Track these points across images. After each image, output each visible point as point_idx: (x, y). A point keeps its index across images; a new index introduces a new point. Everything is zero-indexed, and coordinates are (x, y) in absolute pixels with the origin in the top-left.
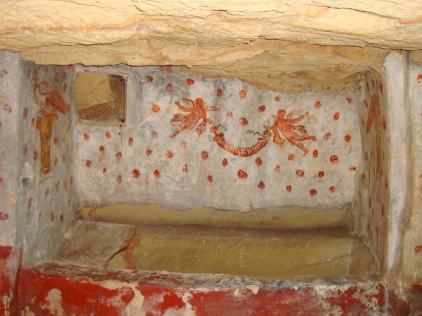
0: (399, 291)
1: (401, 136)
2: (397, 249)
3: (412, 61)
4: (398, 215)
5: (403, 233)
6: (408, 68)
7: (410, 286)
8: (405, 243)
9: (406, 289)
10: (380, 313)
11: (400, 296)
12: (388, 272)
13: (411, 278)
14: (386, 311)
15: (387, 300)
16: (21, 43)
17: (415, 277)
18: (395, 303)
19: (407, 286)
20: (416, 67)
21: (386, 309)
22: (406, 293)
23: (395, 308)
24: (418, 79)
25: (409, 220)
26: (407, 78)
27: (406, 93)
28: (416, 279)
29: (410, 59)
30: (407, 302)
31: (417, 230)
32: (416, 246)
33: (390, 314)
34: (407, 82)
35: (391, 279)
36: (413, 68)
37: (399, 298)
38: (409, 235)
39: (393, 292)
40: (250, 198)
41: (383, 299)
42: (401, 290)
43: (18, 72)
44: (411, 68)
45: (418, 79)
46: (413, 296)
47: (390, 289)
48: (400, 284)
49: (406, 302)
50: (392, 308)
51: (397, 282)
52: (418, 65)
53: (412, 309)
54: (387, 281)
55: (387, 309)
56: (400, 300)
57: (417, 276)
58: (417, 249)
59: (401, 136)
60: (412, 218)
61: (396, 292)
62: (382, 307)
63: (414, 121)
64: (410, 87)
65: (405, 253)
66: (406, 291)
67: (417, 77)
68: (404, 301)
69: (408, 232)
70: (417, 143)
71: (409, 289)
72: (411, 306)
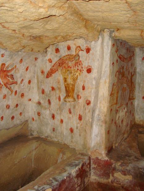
23: (99, 166)
30: (109, 160)
49: (108, 160)
50: (96, 167)
55: (92, 168)
61: (100, 158)
68: (106, 160)
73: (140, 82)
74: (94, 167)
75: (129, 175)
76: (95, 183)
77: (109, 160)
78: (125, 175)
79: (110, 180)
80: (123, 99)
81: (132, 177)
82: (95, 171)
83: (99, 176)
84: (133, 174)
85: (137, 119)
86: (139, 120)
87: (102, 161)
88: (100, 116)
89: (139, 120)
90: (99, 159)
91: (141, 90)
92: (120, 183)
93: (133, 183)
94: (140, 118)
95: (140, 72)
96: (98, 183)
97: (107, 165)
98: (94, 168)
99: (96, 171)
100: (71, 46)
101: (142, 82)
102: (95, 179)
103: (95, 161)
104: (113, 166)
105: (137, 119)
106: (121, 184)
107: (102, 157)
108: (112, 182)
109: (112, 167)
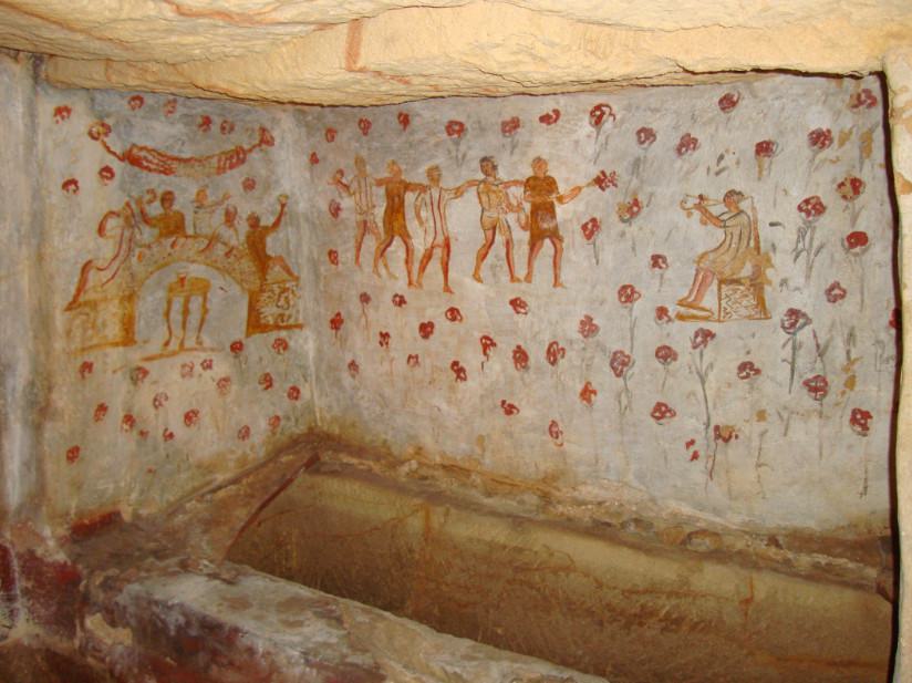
0: (47, 545)
1: (19, 231)
2: (26, 465)
3: (47, 79)
4: (18, 395)
5: (37, 428)
6: (36, 93)
7: (68, 529)
8: (46, 448)
9: (61, 539)
10: (8, 604)
11: (50, 555)
12: (10, 515)
13: (67, 514)
14: (19, 598)
15: (17, 575)
16: (451, 82)
17: (73, 512)
18: (40, 574)
19: (63, 531)
20: (51, 91)
21: (18, 592)
22: (62, 546)
23: (40, 584)
24: (55, 115)
25: (48, 403)
26: (32, 114)
27: (31, 145)
28: (76, 514)
29: (43, 76)
30: (69, 563)
31: (66, 417)
32: (68, 449)
33: (29, 600)
34: (33, 122)
35: (20, 529)
36: (47, 93)
37: (49, 560)
38: (51, 431)
39: (31, 553)
40: (755, 97)
41: (9, 574)
42: (51, 543)
43: (265, 83)
44: (42, 93)
45: (55, 115)
46: (77, 549)
47: (21, 549)
48: (47, 532)
49: (65, 563)
50: (33, 587)
51: (38, 531)
52: (56, 87)
53: (85, 572)
54: (12, 535)
55: (22, 591)
56: (53, 563)
57: (77, 507)
58: (71, 455)
59: (19, 231)
60: (54, 396)
61: (39, 552)
62: (11, 590)
63: (48, 201)
64: (40, 132)
65: (49, 467)
66: (62, 542)
67: (53, 112)
68: (62, 562)
69: (48, 425)
70: (56, 244)
71: (65, 537)
72: (80, 567)
73: (316, 256)
74: (26, 588)
75: (124, 627)
76: (39, 650)
77: (69, 563)
78: (113, 624)
79: (77, 643)
80: (194, 319)
81: (131, 635)
82: (31, 602)
83: (47, 623)
84: (133, 622)
85: (321, 409)
86: (328, 417)
87: (48, 565)
88: (35, 390)
89: (328, 417)
90: (37, 559)
91: (322, 288)
92: (102, 655)
93: (137, 660)
94: (330, 407)
95: (312, 213)
96: (48, 650)
97: (66, 580)
98: (26, 592)
99: (33, 605)
100: (521, 118)
101: (322, 259)
102: (37, 636)
103: (28, 564)
104: (81, 587)
105: (321, 409)
106: (108, 659)
107: (47, 551)
108: (83, 651)
109: (78, 591)
